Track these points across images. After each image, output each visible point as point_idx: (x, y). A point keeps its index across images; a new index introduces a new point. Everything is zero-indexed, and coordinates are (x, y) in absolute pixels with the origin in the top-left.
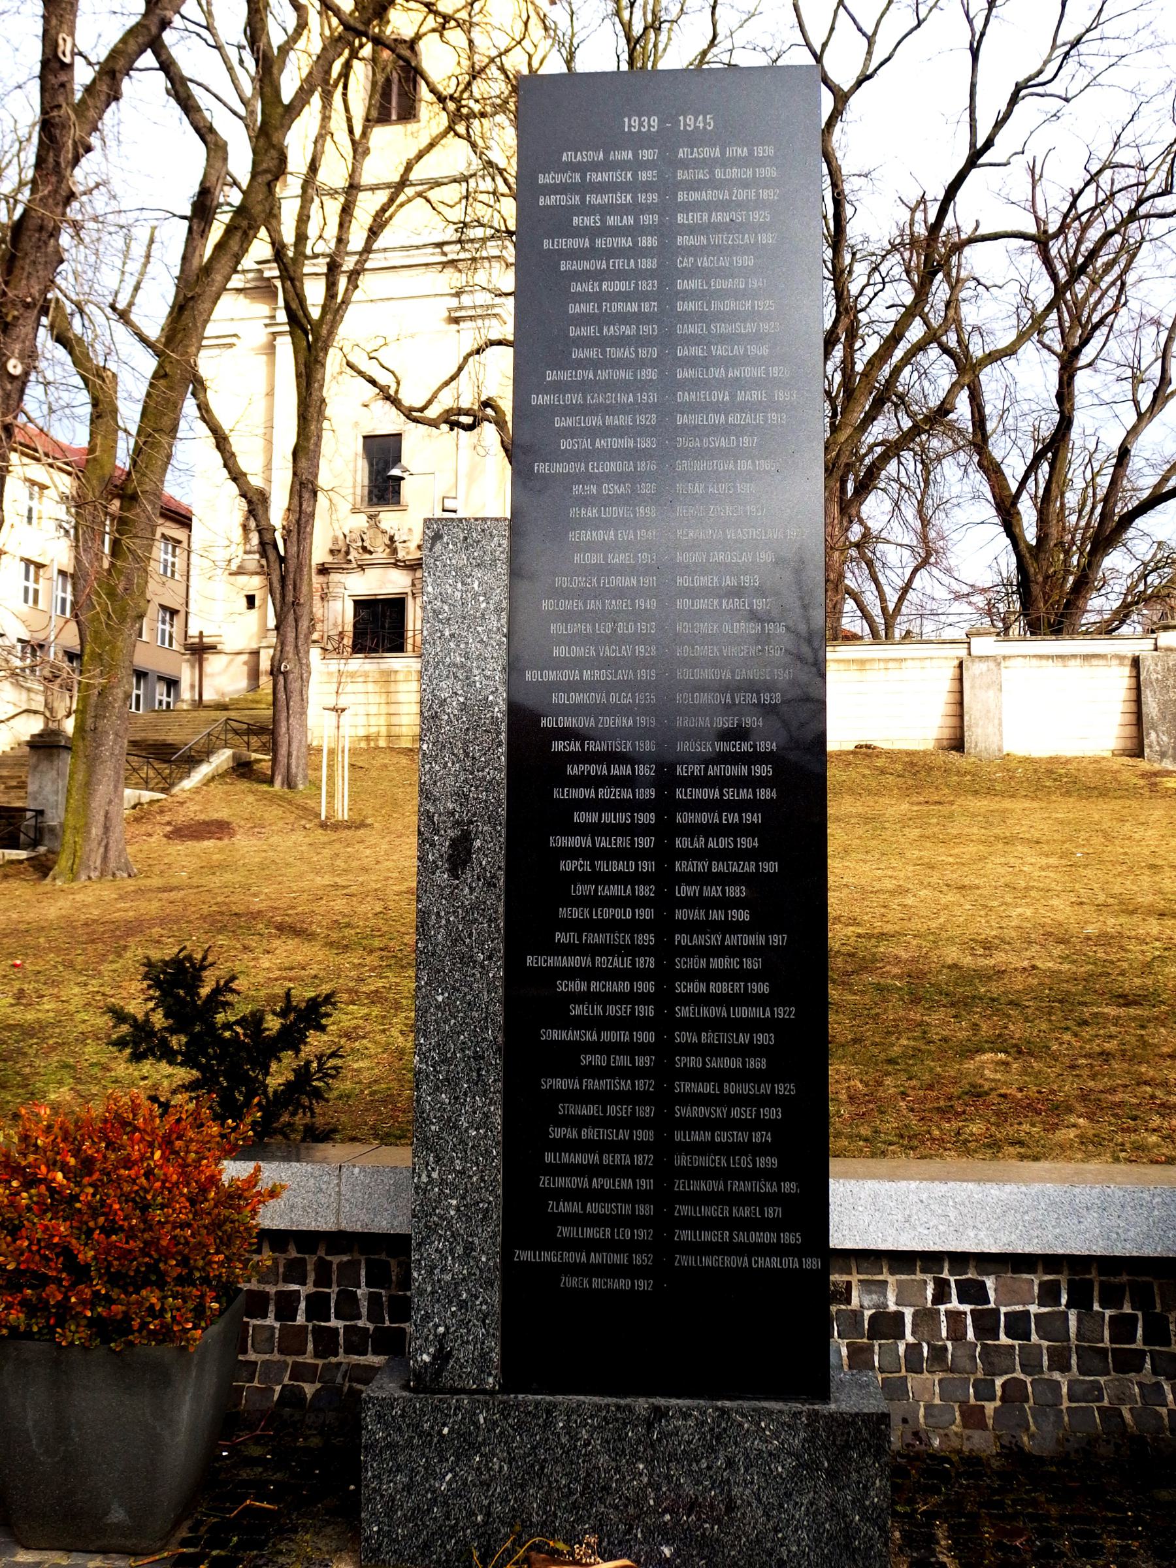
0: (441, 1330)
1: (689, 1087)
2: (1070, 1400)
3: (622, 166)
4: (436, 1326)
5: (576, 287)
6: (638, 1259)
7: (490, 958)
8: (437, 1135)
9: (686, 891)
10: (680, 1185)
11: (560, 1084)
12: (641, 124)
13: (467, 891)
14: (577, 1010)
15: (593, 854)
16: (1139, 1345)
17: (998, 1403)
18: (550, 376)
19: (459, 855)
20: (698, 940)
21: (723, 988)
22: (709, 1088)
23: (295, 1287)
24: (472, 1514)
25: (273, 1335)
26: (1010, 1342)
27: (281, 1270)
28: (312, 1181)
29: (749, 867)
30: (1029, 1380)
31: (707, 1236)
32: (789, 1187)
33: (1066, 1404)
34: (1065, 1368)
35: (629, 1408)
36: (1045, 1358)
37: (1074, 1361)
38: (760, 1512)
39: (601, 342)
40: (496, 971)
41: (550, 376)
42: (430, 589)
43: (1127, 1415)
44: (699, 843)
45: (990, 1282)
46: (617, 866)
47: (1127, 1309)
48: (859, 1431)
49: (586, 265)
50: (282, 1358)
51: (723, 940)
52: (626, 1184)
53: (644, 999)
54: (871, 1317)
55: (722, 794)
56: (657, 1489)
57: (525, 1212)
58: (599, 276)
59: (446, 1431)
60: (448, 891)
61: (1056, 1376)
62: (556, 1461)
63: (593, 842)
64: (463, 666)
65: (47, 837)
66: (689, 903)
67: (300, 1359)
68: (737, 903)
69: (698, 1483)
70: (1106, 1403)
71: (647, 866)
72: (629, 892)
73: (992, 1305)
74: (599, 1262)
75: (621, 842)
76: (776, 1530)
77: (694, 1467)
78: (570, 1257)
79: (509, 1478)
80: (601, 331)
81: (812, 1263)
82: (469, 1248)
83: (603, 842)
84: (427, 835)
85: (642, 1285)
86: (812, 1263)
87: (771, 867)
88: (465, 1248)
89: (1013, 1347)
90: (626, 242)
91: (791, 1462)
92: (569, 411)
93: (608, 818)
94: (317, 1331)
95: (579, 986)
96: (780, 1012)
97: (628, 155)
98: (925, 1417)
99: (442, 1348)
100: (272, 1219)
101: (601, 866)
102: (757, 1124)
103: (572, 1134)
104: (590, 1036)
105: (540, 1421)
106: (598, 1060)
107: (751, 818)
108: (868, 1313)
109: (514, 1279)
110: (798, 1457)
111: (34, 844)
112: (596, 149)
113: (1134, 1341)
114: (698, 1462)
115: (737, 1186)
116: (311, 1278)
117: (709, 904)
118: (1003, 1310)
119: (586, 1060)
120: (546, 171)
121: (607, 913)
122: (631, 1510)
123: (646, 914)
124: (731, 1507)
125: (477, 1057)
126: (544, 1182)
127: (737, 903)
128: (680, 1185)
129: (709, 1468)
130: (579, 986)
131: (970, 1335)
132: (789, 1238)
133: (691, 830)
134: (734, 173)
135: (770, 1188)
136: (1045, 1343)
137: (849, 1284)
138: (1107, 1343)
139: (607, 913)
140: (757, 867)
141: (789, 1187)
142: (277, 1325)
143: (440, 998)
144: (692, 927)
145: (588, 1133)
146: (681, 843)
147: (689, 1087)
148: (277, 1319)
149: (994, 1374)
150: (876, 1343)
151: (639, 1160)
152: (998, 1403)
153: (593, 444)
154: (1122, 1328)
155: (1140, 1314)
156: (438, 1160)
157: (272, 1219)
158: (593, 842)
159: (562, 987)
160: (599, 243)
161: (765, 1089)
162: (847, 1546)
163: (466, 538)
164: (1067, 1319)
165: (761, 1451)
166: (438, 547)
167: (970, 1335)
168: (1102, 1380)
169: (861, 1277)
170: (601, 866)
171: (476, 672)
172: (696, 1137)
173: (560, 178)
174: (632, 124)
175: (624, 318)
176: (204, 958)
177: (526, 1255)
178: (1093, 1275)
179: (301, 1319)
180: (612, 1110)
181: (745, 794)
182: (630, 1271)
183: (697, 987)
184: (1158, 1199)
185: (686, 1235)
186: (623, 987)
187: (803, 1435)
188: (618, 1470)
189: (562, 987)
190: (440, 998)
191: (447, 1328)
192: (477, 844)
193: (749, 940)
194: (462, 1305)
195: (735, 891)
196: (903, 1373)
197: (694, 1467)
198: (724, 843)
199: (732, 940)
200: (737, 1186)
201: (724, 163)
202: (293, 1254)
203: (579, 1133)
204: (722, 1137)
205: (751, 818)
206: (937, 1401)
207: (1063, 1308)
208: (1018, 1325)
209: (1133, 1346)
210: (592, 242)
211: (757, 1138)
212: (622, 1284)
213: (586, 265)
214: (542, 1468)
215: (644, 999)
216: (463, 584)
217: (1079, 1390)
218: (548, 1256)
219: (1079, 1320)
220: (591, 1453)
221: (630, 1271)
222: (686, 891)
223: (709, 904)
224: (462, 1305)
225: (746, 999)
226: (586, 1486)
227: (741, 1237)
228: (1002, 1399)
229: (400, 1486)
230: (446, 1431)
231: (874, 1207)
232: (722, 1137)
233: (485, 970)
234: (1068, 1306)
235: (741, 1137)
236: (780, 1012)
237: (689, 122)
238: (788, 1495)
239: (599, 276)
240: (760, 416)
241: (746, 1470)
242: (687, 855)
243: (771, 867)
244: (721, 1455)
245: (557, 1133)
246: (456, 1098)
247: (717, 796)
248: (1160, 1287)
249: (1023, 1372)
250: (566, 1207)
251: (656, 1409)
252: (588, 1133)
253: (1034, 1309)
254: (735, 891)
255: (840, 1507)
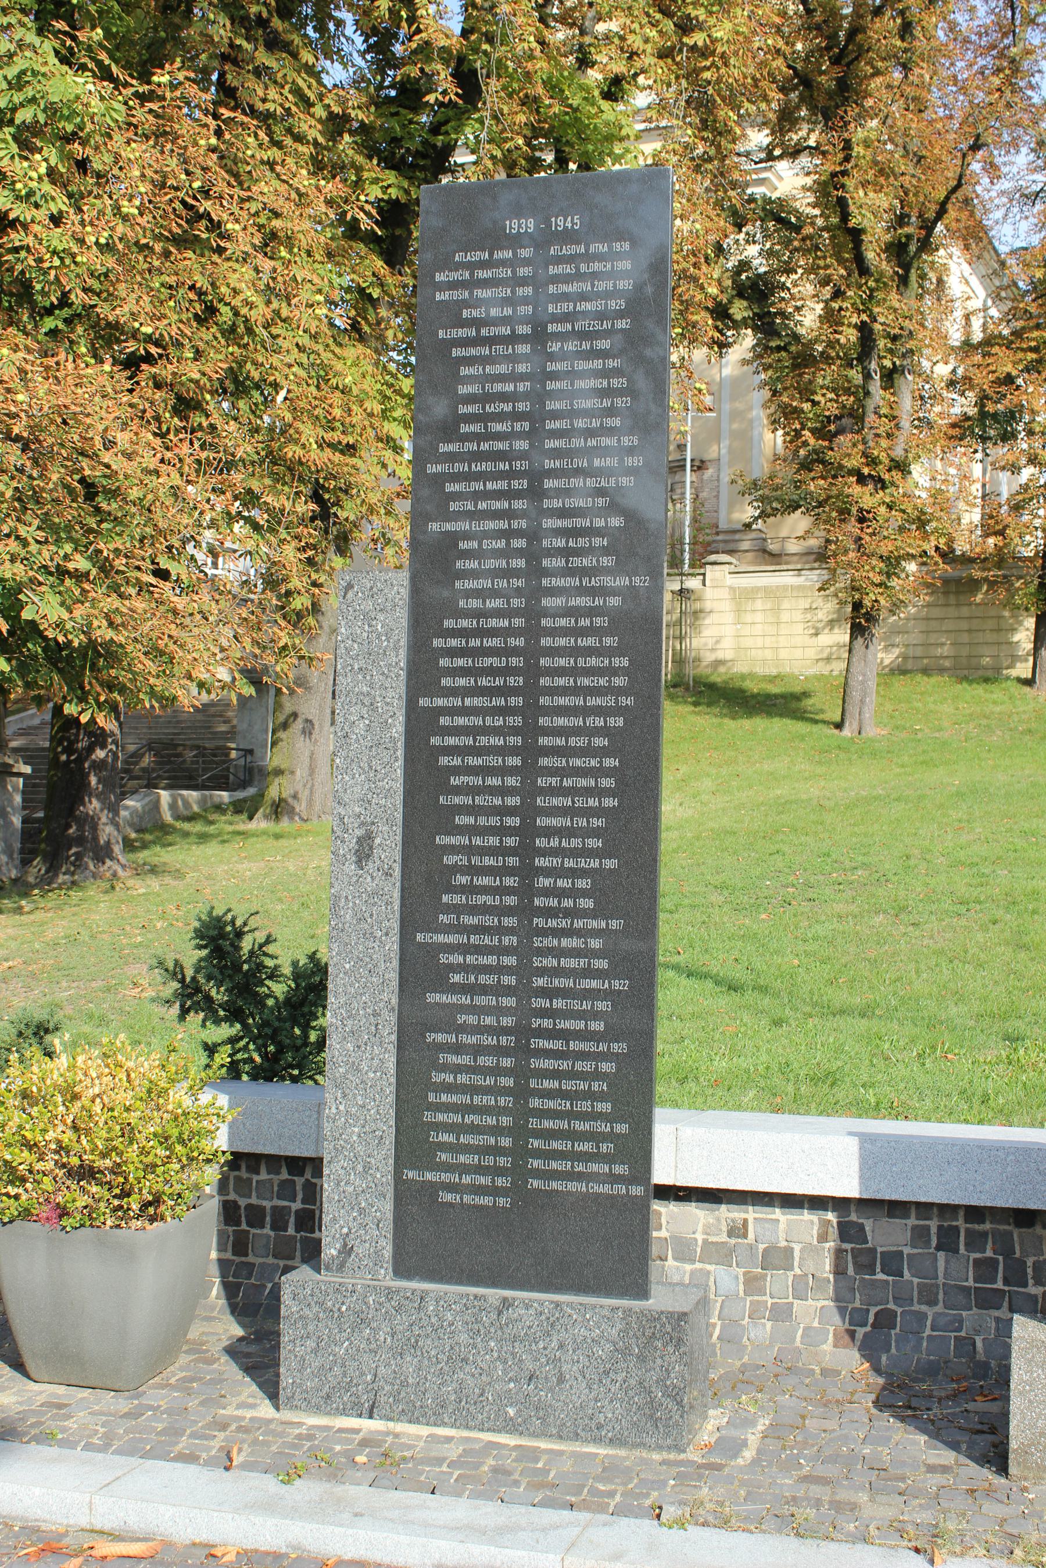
0: (345, 1230)
1: (544, 1044)
2: (932, 1330)
3: (503, 263)
4: (342, 1227)
5: (465, 371)
6: (500, 1182)
7: (387, 934)
8: (344, 1076)
9: (545, 882)
10: (533, 1123)
11: (440, 1038)
12: (520, 226)
13: (369, 879)
14: (456, 978)
15: (470, 850)
16: (999, 1285)
17: (868, 1328)
18: (444, 448)
19: (364, 852)
20: (552, 923)
21: (572, 963)
22: (557, 1045)
23: (286, 1203)
24: (363, 1374)
25: (268, 1243)
26: (885, 1277)
27: (276, 1189)
28: (296, 1115)
29: (595, 864)
30: (899, 1310)
31: (554, 1165)
32: (621, 1128)
33: (928, 1332)
34: (932, 1302)
35: (483, 1298)
36: (915, 1293)
37: (941, 1296)
38: (584, 1385)
39: (483, 418)
40: (393, 944)
41: (444, 448)
42: (343, 630)
43: (979, 1344)
44: (554, 843)
45: (868, 1225)
46: (489, 861)
47: (989, 1253)
48: (663, 1325)
49: (473, 351)
50: (276, 1261)
51: (572, 923)
52: (491, 1121)
53: (508, 970)
54: (765, 1250)
55: (573, 802)
56: (505, 1362)
57: (412, 1144)
58: (484, 360)
59: (344, 1308)
60: (355, 879)
61: (924, 1308)
62: (427, 1336)
63: (470, 841)
64: (369, 694)
65: (257, 777)
66: (547, 892)
67: (978, 1255)
68: (584, 893)
69: (536, 1360)
70: (963, 1334)
71: (512, 861)
72: (498, 883)
73: (870, 1245)
74: (465, 1183)
75: (493, 841)
76: (596, 1400)
77: (534, 1347)
78: (445, 1177)
79: (391, 1348)
80: (484, 408)
81: (637, 1190)
82: (367, 1167)
83: (478, 841)
84: (339, 833)
85: (502, 1201)
86: (637, 1190)
87: (611, 864)
88: (364, 1167)
89: (887, 1282)
90: (505, 331)
91: (609, 1347)
92: (456, 478)
93: (482, 821)
94: (304, 1240)
95: (457, 959)
96: (617, 985)
97: (508, 254)
98: (802, 1337)
99: (345, 1245)
100: (264, 1145)
101: (475, 860)
102: (597, 1075)
103: (449, 1078)
104: (465, 1000)
105: (416, 1305)
106: (472, 1020)
107: (597, 822)
108: (762, 1247)
109: (401, 1186)
110: (614, 1344)
111: (244, 785)
112: (483, 250)
113: (967, 1280)
114: (537, 1343)
115: (580, 1126)
116: (300, 1196)
117: (561, 894)
118: (879, 1250)
119: (461, 1019)
120: (441, 270)
121: (481, 899)
122: (484, 1378)
123: (511, 900)
124: (561, 1380)
125: (375, 1014)
126: (428, 1116)
127: (584, 893)
128: (533, 1123)
129: (545, 1348)
130: (457, 959)
131: (851, 1271)
132: (619, 1169)
133: (549, 832)
134: (596, 266)
135: (604, 1128)
136: (916, 1280)
137: (745, 1221)
138: (971, 1283)
139: (481, 899)
140: (601, 864)
141: (621, 1128)
142: (272, 1233)
143: (347, 966)
144: (549, 913)
145: (463, 1079)
146: (540, 842)
147: (544, 1044)
148: (273, 1228)
149: (870, 1305)
150: (769, 1273)
151: (502, 1101)
152: (868, 1328)
153: (476, 506)
154: (985, 1269)
155: (1001, 1258)
156: (345, 1096)
157: (264, 1145)
158: (470, 841)
159: (443, 959)
160: (583, 268)
161: (603, 1047)
162: (651, 1416)
163: (371, 588)
164: (936, 1259)
165: (585, 1338)
166: (350, 594)
167: (851, 1271)
168: (964, 1313)
169: (757, 1216)
170: (475, 860)
171: (378, 699)
172: (547, 1084)
173: (455, 276)
174: (513, 226)
175: (504, 397)
176: (245, 924)
177: (411, 1174)
178: (960, 1223)
179: (291, 1231)
180: (482, 1060)
181: (593, 802)
182: (495, 1191)
183: (551, 962)
184: (1012, 1157)
185: (536, 1163)
186: (491, 960)
187: (619, 1326)
188: (475, 1346)
189: (443, 959)
190: (347, 966)
191: (350, 1229)
192: (378, 841)
193: (594, 924)
194: (362, 1211)
195: (582, 884)
196: (791, 1299)
197: (534, 1347)
198: (575, 843)
199: (579, 924)
200: (580, 1126)
201: (588, 257)
202: (284, 1175)
203: (455, 1078)
204: (568, 1085)
205: (597, 822)
206: (816, 1324)
207: (932, 1250)
208: (892, 1263)
209: (994, 1286)
210: (478, 331)
211: (596, 1086)
212: (486, 1201)
213: (473, 351)
214: (417, 1342)
215: (508, 970)
216: (370, 626)
217: (942, 1321)
218: (429, 1176)
219: (947, 1262)
220: (453, 1332)
221: (495, 1191)
222: (545, 882)
223: (561, 894)
224: (362, 1211)
225: (589, 973)
226: (450, 1358)
227: (580, 1168)
228: (873, 1326)
229: (309, 1350)
230: (344, 1308)
231: (685, 1145)
232: (568, 1085)
233: (382, 944)
234: (938, 1248)
235: (583, 1086)
236: (617, 985)
237: (560, 223)
238: (607, 1373)
239: (484, 360)
240: (612, 480)
241: (574, 1351)
242: (544, 853)
243: (611, 864)
244: (555, 1338)
245: (438, 1077)
246: (359, 1047)
247: (570, 803)
248: (1020, 1236)
249: (895, 1304)
250: (446, 1138)
251: (505, 1300)
252: (463, 1079)
253: (907, 1250)
254: (582, 884)
255: (646, 1384)
